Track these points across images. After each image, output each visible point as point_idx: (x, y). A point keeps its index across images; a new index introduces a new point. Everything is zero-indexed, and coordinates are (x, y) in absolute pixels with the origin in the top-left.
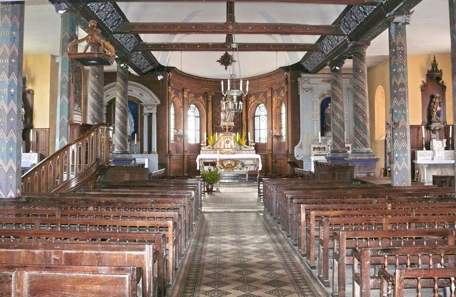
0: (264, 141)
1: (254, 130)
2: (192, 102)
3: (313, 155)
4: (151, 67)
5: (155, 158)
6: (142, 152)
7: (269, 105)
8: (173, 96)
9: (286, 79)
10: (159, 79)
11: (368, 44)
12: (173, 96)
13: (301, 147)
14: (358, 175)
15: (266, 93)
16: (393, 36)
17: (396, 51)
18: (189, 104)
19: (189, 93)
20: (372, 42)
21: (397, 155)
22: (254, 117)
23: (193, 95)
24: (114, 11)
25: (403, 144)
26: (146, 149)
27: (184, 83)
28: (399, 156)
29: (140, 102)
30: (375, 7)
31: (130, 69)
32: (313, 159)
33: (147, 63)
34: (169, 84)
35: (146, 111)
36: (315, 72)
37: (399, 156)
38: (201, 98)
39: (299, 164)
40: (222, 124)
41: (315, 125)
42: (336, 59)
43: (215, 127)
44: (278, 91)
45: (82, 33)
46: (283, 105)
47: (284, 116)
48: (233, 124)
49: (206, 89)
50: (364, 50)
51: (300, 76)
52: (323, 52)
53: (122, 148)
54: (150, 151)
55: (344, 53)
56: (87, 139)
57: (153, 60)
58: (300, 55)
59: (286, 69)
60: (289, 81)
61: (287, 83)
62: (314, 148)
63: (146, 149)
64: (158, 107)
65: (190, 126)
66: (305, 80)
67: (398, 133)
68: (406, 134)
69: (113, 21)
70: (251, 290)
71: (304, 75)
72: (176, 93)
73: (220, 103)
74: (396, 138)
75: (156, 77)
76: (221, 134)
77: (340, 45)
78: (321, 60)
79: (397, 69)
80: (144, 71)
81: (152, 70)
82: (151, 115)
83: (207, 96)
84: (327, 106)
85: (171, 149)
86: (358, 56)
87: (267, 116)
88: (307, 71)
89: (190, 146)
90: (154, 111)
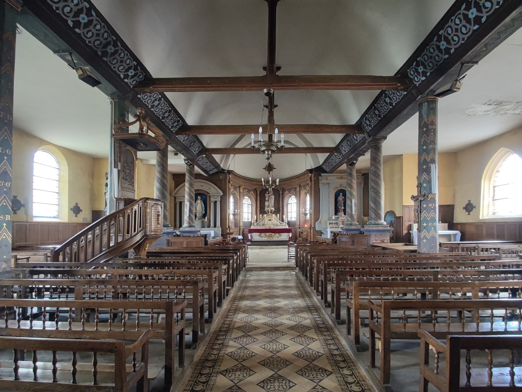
0: (294, 219)
1: (287, 212)
2: (246, 195)
3: (329, 228)
4: (215, 170)
5: (219, 230)
6: (209, 226)
7: (298, 197)
8: (232, 190)
9: (311, 178)
10: (462, 350)
11: (385, 138)
12: (232, 190)
13: (320, 223)
14: (373, 242)
15: (296, 188)
16: (425, 116)
17: (427, 130)
18: (244, 196)
19: (244, 189)
20: (389, 137)
21: (425, 224)
22: (288, 204)
23: (247, 190)
24: (170, 111)
25: (431, 215)
26: (212, 224)
27: (240, 182)
28: (427, 225)
29: (209, 193)
30: (405, 93)
31: (197, 169)
32: (329, 230)
33: (212, 167)
34: (229, 182)
35: (212, 199)
36: (331, 172)
37: (427, 225)
38: (252, 192)
39: (320, 233)
40: (266, 209)
41: (331, 206)
42: (357, 151)
43: (261, 210)
44: (305, 187)
45: (131, 119)
46: (308, 195)
47: (308, 203)
48: (273, 209)
49: (255, 187)
50: (380, 143)
51: (321, 175)
52: (341, 153)
53: (189, 223)
54: (215, 226)
55: (361, 150)
56: (129, 211)
57: (216, 165)
58: (322, 157)
59: (311, 171)
60: (313, 179)
61: (311, 181)
62: (330, 223)
63: (212, 224)
64: (221, 197)
65: (243, 210)
66: (324, 178)
67: (427, 204)
68: (435, 205)
69: (173, 121)
70: (271, 359)
71: (323, 174)
72: (235, 188)
73: (265, 196)
74: (425, 209)
75: (219, 177)
76: (265, 215)
77: (358, 143)
78: (338, 161)
79: (427, 146)
80: (211, 173)
81: (216, 173)
82: (215, 202)
83: (257, 192)
84: (339, 195)
85: (230, 225)
86: (376, 149)
87: (297, 203)
88: (325, 172)
89: (244, 223)
90: (218, 200)
